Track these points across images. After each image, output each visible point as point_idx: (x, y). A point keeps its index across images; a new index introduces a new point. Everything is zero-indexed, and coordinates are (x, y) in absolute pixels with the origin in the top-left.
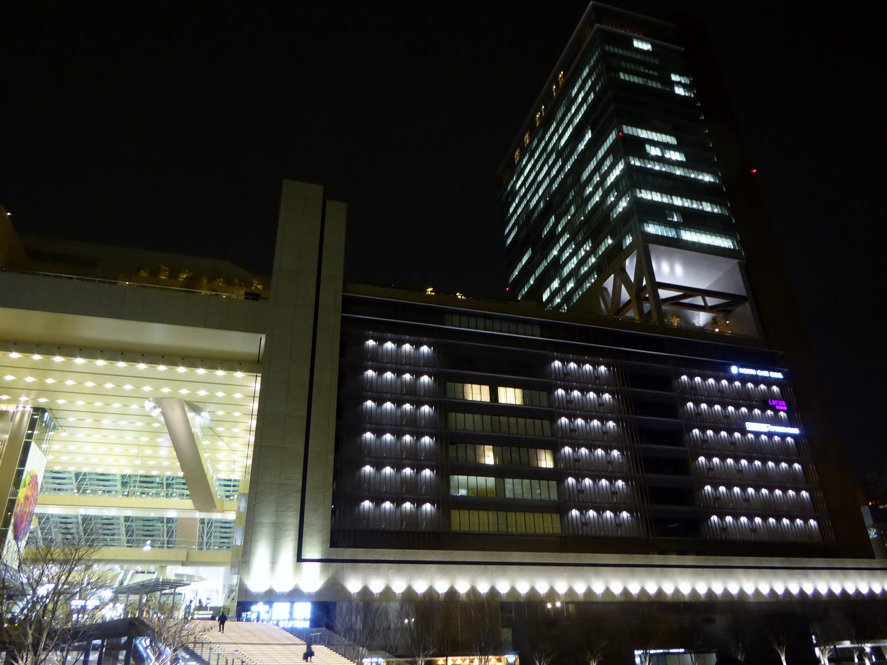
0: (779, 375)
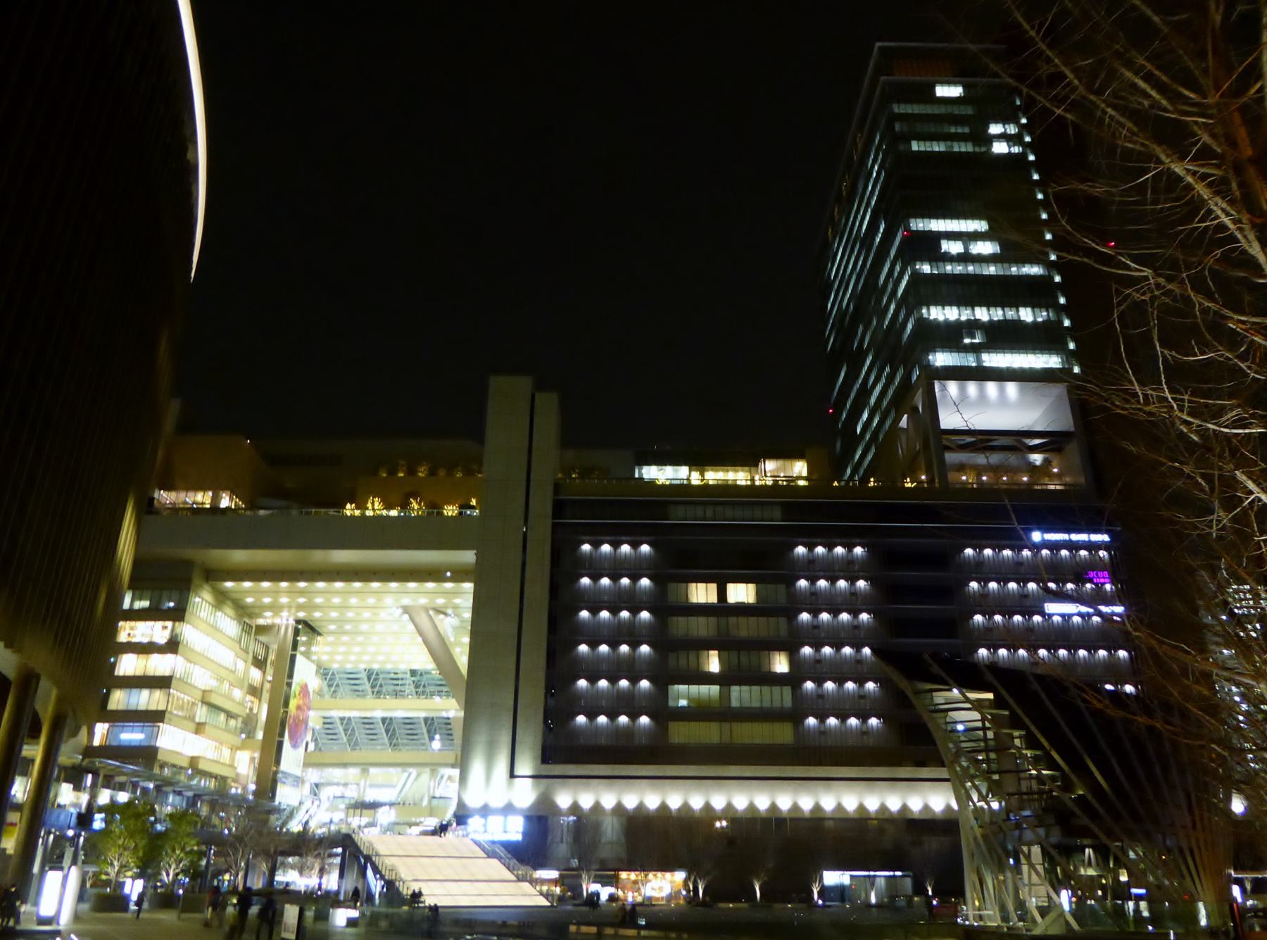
0: (1106, 538)
